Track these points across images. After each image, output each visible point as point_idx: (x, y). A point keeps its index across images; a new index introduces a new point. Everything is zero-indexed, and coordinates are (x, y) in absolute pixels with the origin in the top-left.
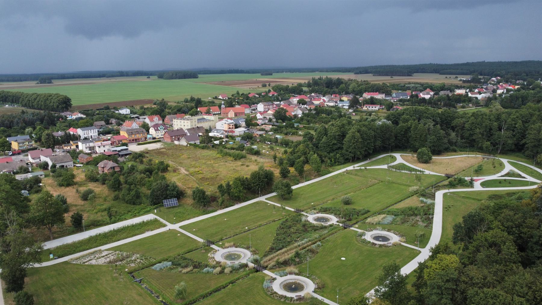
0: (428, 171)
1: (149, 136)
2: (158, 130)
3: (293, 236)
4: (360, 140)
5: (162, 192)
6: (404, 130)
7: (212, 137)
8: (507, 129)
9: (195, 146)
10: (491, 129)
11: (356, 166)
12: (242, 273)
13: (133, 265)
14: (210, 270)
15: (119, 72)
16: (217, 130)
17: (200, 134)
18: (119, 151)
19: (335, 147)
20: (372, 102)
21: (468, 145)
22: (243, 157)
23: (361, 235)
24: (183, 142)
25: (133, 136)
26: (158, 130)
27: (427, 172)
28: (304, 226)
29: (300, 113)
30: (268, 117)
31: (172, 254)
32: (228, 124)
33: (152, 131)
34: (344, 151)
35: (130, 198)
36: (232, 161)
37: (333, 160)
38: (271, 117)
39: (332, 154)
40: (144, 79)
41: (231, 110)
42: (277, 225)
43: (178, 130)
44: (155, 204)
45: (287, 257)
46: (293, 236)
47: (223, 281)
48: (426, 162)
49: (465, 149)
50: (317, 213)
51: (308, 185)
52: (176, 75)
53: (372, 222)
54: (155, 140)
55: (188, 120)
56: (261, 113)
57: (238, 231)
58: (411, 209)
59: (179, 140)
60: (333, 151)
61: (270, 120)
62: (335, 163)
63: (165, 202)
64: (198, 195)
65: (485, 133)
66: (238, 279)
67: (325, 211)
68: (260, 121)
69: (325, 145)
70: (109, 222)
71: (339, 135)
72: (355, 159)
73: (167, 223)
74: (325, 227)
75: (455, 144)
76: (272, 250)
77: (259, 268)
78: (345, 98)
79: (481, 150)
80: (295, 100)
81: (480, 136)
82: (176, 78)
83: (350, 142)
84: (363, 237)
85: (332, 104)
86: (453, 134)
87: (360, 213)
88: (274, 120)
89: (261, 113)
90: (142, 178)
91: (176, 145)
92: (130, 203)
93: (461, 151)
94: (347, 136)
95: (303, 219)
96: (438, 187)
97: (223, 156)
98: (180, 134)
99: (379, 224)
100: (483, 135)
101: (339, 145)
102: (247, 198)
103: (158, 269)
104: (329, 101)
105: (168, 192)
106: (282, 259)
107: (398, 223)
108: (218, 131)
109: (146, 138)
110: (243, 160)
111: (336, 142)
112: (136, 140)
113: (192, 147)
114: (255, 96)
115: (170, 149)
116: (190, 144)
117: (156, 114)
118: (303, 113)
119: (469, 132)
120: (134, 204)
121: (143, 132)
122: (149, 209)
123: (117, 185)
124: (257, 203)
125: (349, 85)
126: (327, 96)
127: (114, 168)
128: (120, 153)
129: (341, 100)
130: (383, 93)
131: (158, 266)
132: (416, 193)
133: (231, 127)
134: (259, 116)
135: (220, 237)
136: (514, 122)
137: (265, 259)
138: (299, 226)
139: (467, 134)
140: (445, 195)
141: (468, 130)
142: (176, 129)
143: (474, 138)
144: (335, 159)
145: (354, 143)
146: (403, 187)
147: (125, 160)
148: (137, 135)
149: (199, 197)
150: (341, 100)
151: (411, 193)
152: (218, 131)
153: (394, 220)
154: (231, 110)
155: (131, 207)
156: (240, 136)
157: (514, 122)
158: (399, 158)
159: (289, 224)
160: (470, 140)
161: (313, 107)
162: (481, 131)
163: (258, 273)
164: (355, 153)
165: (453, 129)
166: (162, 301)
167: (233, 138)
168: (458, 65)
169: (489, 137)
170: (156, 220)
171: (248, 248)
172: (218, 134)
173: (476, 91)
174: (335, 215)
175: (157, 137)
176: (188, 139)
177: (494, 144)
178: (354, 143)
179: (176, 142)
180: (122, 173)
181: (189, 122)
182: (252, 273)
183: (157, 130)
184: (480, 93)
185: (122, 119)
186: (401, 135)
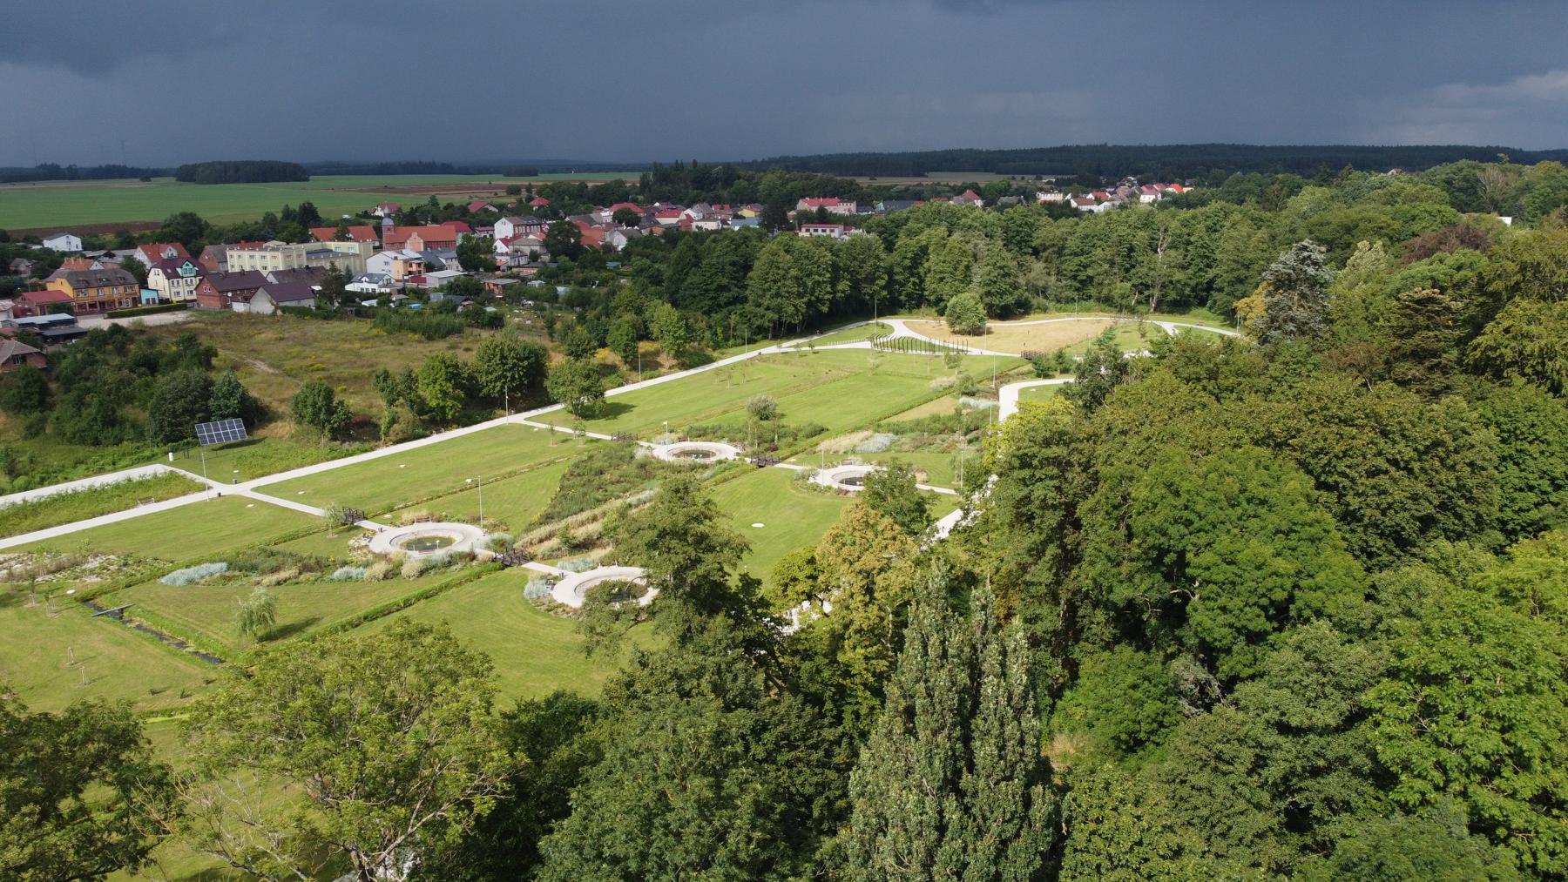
0: (975, 348)
1: (145, 295)
2: (178, 276)
3: (610, 488)
4: (793, 272)
5: (194, 402)
6: (910, 255)
7: (355, 294)
8: (1172, 246)
9: (302, 313)
10: (1131, 249)
11: (788, 346)
12: (456, 572)
13: (94, 580)
14: (353, 571)
15: (44, 166)
16: (371, 276)
17: (317, 288)
18: (42, 326)
19: (724, 297)
20: (823, 218)
21: (1075, 295)
22: (458, 331)
23: (805, 477)
24: (262, 305)
25: (92, 292)
26: (178, 276)
27: (974, 351)
28: (642, 466)
29: (620, 242)
30: (527, 250)
31: (228, 550)
32: (405, 261)
33: (157, 279)
34: (749, 307)
35: (84, 424)
36: (420, 341)
37: (719, 330)
38: (537, 248)
39: (716, 316)
40: (136, 184)
41: (415, 234)
42: (564, 468)
43: (242, 273)
44: (168, 439)
45: (594, 528)
46: (610, 488)
47: (395, 593)
48: (977, 331)
49: (1069, 306)
50: (680, 440)
51: (650, 388)
52: (237, 170)
53: (835, 448)
54: (165, 306)
55: (273, 249)
56: (506, 241)
57: (442, 488)
58: (936, 419)
59: (247, 300)
60: (720, 306)
61: (534, 257)
62: (727, 340)
63: (203, 430)
64: (310, 401)
65: (1118, 260)
66: (447, 587)
67: (702, 434)
68: (504, 259)
69: (696, 292)
70: (9, 487)
71: (734, 264)
72: (782, 330)
73: (210, 482)
74: (705, 467)
75: (1043, 292)
76: (548, 518)
77: (509, 557)
78: (748, 213)
79: (1107, 302)
80: (606, 215)
81: (1106, 266)
82: (235, 181)
83: (766, 280)
84: (811, 480)
85: (711, 226)
86: (1038, 266)
87: (800, 435)
88: (547, 258)
89: (506, 241)
90: (122, 381)
91: (239, 315)
92: (83, 442)
93: (1059, 310)
94: (757, 263)
95: (640, 454)
96: (1004, 378)
97: (390, 333)
98: (248, 284)
99: (854, 452)
100: (1112, 263)
101: (735, 291)
102: (469, 417)
103: (180, 582)
104: (704, 219)
105: (211, 402)
106: (580, 533)
107: (906, 447)
108: (372, 278)
109: (137, 301)
110: (452, 339)
111: (725, 281)
112: (102, 304)
113: (291, 317)
114: (486, 210)
115: (218, 324)
116: (284, 310)
117: (169, 242)
118: (630, 239)
119: (1076, 260)
120: (96, 443)
121: (125, 283)
122: (147, 453)
123: (36, 398)
124: (499, 428)
125: (757, 184)
126: (697, 206)
127: (24, 358)
128: (47, 333)
129: (737, 217)
130: (850, 200)
131: (180, 576)
132: (948, 390)
133: (414, 268)
134: (500, 247)
135: (385, 503)
136: (1185, 230)
137: (527, 538)
138: (630, 469)
139: (1071, 265)
140: (1022, 392)
141: (1076, 254)
142: (237, 270)
143: (1090, 272)
144: (726, 328)
145: (775, 282)
146: (914, 382)
147: (64, 350)
148: (107, 291)
149: (314, 404)
150: (737, 217)
151: (935, 391)
152: (372, 278)
153: (893, 442)
154: (415, 234)
155: (82, 451)
156: (441, 289)
157: (1185, 230)
158: (899, 326)
159: (597, 465)
160: (1081, 282)
161: (658, 231)
162: (1109, 253)
163: (507, 570)
164: (779, 310)
165: (1036, 252)
166: (196, 653)
167: (421, 295)
168: (1041, 150)
169: (1127, 271)
170: (173, 477)
171: (475, 520)
172: (375, 286)
173: (1091, 196)
174: (732, 440)
175: (175, 299)
176: (275, 293)
177: (1143, 287)
178: (775, 282)
179: (239, 307)
180: (54, 374)
181: (279, 255)
182: (490, 571)
183: (172, 276)
184: (1099, 201)
185: (51, 263)
186: (905, 268)
